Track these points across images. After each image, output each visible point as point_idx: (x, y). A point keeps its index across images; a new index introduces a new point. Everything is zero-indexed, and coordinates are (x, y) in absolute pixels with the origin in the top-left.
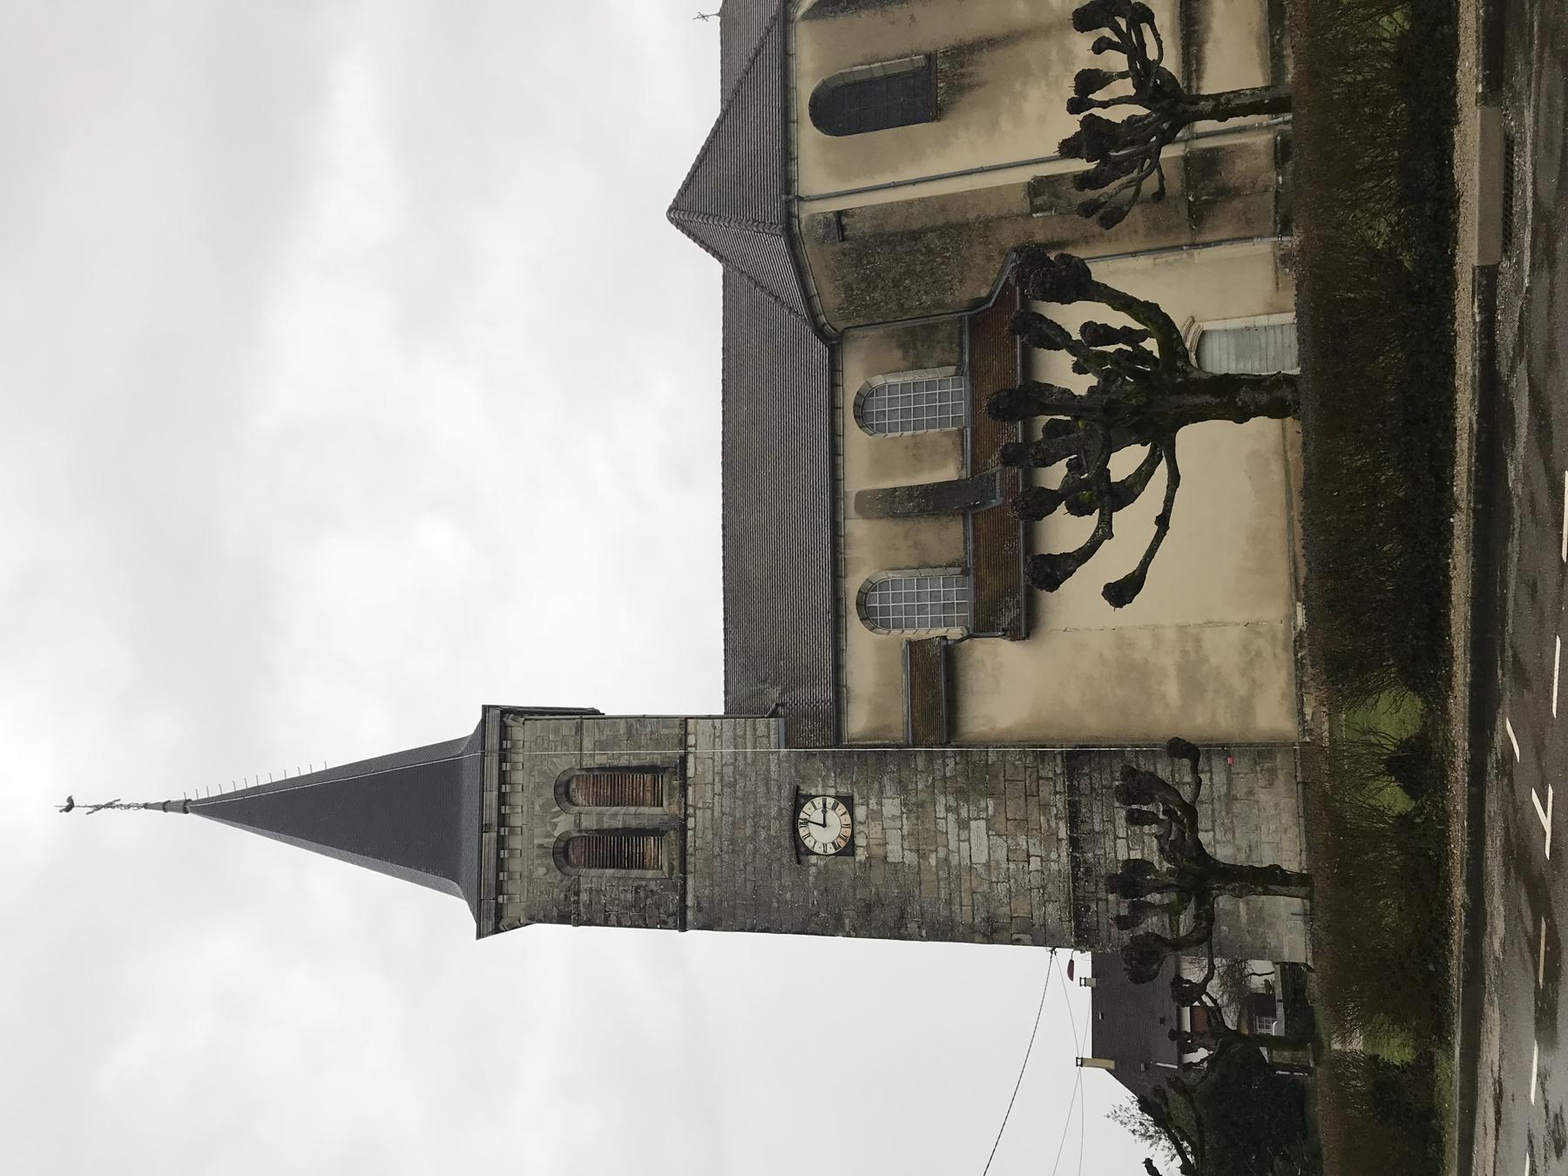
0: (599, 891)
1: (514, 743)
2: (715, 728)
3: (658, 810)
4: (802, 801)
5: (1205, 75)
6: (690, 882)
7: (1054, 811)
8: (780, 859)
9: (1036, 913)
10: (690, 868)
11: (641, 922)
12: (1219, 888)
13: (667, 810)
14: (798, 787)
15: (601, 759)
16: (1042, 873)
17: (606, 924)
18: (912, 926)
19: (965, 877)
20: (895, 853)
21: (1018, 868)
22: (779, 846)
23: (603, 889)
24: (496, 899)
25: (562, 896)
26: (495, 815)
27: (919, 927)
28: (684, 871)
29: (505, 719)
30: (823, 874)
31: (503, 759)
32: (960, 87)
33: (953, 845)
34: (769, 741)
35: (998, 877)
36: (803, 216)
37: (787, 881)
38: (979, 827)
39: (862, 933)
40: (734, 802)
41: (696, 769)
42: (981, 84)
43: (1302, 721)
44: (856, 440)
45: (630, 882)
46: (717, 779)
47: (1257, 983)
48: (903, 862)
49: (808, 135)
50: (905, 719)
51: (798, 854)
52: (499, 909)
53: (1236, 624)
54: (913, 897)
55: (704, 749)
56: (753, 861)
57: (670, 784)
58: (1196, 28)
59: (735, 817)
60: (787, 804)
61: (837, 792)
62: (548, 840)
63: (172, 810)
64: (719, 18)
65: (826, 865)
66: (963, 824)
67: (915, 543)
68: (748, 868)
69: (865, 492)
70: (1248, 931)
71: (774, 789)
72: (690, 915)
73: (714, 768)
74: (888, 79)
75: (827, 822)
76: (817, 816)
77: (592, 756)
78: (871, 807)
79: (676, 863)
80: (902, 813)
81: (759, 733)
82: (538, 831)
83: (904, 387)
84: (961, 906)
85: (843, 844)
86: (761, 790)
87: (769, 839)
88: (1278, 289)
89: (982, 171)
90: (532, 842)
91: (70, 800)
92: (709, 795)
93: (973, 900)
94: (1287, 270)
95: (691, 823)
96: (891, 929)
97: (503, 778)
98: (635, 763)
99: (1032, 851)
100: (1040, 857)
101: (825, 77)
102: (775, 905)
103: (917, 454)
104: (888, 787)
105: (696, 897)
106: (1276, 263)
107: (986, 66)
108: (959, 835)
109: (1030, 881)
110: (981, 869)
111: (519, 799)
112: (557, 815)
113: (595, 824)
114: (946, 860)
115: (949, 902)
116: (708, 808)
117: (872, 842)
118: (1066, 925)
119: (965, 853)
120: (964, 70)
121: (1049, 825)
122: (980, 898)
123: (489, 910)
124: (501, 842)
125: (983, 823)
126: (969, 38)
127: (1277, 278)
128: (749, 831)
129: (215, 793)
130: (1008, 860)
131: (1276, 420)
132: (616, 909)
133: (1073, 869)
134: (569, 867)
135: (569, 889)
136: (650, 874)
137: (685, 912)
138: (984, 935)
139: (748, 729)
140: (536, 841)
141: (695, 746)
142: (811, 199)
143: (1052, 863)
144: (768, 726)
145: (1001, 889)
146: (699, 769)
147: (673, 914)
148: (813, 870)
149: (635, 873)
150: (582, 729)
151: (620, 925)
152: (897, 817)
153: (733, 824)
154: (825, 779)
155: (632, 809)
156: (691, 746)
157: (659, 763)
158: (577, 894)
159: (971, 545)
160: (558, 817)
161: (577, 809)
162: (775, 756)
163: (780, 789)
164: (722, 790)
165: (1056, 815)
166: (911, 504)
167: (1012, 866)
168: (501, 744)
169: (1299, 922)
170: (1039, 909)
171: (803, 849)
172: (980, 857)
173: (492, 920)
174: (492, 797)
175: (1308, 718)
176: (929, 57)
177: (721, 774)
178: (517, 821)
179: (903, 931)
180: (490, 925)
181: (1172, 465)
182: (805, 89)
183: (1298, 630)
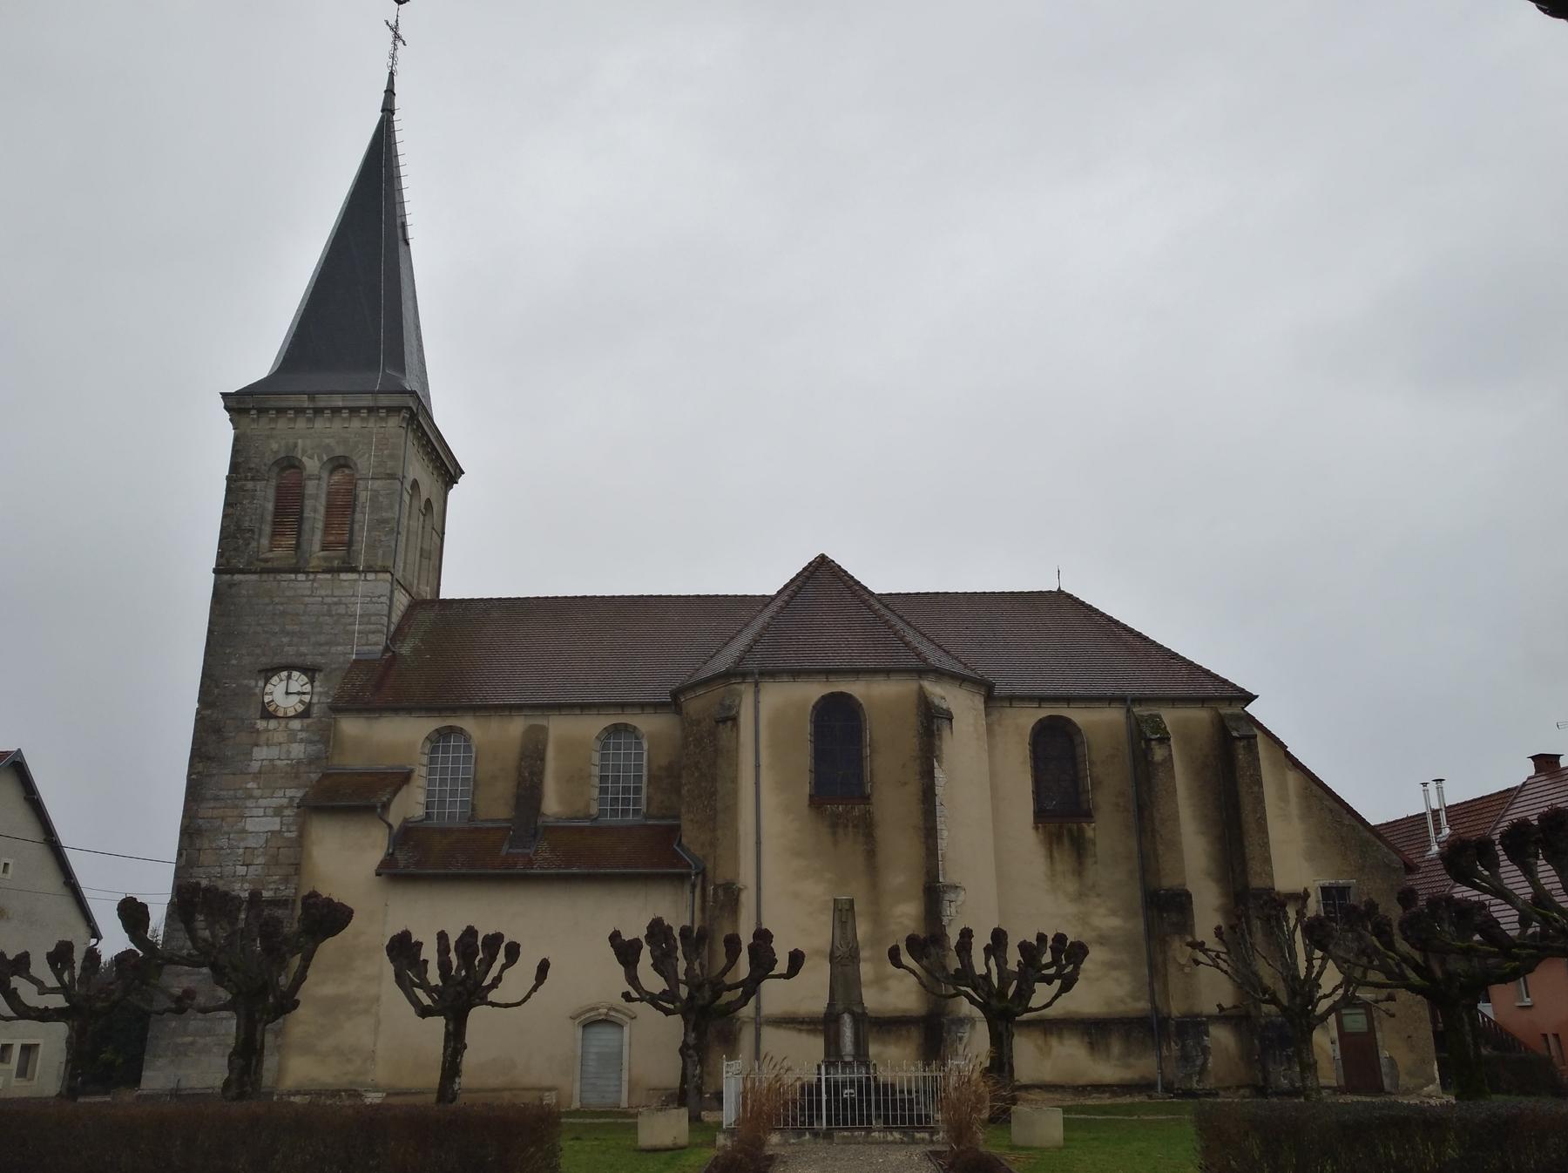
0: (253, 498)
2: (379, 597)
3: (316, 547)
4: (310, 674)
6: (254, 577)
7: (282, 888)
9: (201, 870)
10: (265, 577)
12: (73, 1026)
13: (315, 556)
14: (320, 671)
15: (363, 496)
16: (233, 877)
18: (200, 767)
19: (236, 812)
20: (261, 753)
23: (255, 502)
24: (253, 408)
25: (253, 466)
26: (322, 404)
27: (199, 773)
28: (263, 571)
29: (404, 411)
31: (371, 410)
32: (835, 824)
33: (263, 802)
34: (363, 645)
36: (743, 687)
38: (274, 822)
41: (345, 581)
43: (290, 1094)
44: (592, 726)
45: (258, 525)
47: (1439, 1029)
48: (251, 760)
49: (814, 691)
51: (267, 670)
52: (246, 411)
55: (361, 588)
56: (266, 632)
57: (335, 558)
59: (302, 616)
60: (309, 660)
61: (314, 704)
62: (300, 451)
64: (1056, 590)
65: (255, 694)
66: (278, 812)
69: (547, 734)
70: (169, 1044)
71: (322, 650)
72: (227, 577)
73: (346, 596)
75: (290, 696)
77: (366, 489)
78: (299, 733)
79: (269, 565)
80: (292, 760)
81: (370, 636)
83: (638, 767)
84: (213, 808)
85: (271, 709)
86: (322, 639)
88: (650, 1090)
89: (758, 843)
90: (300, 438)
92: (323, 593)
93: (215, 818)
94: (664, 1098)
95: (301, 577)
97: (354, 411)
98: (356, 527)
99: (251, 868)
100: (246, 875)
101: (864, 706)
104: (314, 748)
105: (240, 582)
106: (671, 1089)
108: (270, 807)
110: (240, 825)
111: (337, 425)
112: (320, 459)
113: (310, 492)
114: (251, 797)
115: (216, 798)
116: (312, 592)
119: (255, 812)
120: (850, 829)
121: (271, 883)
124: (300, 411)
125: (277, 827)
127: (659, 1089)
128: (289, 628)
129: (398, 136)
130: (246, 848)
131: (438, 1080)
132: (238, 513)
135: (258, 471)
136: (265, 542)
138: (187, 826)
139: (375, 626)
140: (300, 441)
141: (366, 580)
142: (757, 693)
144: (376, 644)
145: (224, 842)
146: (346, 584)
147: (228, 562)
148: (253, 683)
149: (267, 529)
150: (392, 479)
151: (225, 516)
152: (288, 756)
153: (298, 614)
154: (326, 693)
155: (320, 525)
156: (365, 576)
157: (353, 548)
158: (253, 479)
159: (489, 825)
160: (319, 460)
161: (325, 475)
162: (349, 651)
163: (322, 655)
164: (325, 604)
165: (279, 889)
166: (527, 774)
169: (172, 1085)
170: (204, 873)
171: (269, 674)
172: (250, 825)
173: (239, 404)
174: (338, 401)
176: (866, 799)
178: (319, 424)
180: (235, 405)
181: (33, 1014)
182: (856, 688)
183: (364, 1094)
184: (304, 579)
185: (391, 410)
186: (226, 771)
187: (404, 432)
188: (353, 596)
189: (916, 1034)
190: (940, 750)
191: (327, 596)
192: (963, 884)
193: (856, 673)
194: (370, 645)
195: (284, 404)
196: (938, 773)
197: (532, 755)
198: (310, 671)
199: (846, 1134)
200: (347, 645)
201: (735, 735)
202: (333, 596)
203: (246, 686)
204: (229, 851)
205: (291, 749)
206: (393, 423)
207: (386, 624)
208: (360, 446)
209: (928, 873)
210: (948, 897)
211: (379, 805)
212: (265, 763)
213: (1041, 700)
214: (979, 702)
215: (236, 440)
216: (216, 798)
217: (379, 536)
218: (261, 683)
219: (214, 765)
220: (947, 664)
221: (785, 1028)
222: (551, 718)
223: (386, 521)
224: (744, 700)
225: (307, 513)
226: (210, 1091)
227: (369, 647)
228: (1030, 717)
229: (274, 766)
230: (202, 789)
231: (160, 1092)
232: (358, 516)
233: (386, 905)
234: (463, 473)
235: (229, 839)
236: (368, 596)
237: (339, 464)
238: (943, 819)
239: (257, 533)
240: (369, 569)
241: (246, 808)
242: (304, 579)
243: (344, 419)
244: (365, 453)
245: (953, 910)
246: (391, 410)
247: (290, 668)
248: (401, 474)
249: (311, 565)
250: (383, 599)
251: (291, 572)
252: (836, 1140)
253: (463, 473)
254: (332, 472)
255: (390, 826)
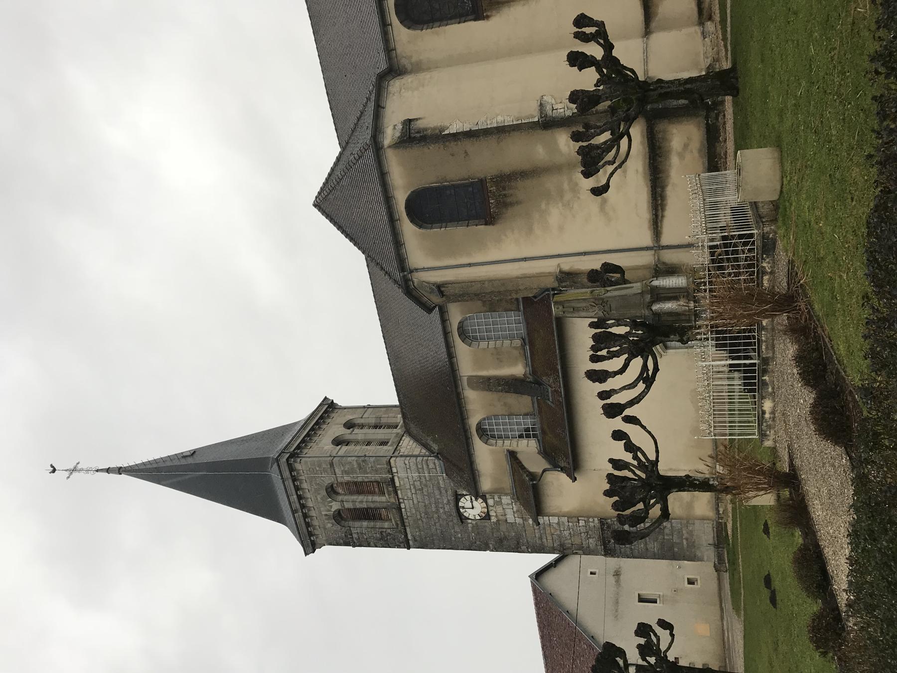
1: (298, 471)
2: (406, 464)
3: (383, 499)
5: (667, 208)
6: (408, 530)
8: (452, 521)
10: (407, 524)
11: (387, 545)
14: (456, 491)
15: (347, 478)
16: (586, 527)
17: (369, 546)
18: (524, 548)
19: (548, 528)
20: (510, 518)
21: (574, 526)
22: (451, 515)
24: (310, 539)
25: (343, 535)
30: (476, 527)
32: (505, 204)
35: (564, 528)
36: (415, 280)
37: (457, 529)
39: (499, 550)
40: (424, 498)
41: (400, 483)
42: (518, 203)
46: (412, 487)
48: (516, 523)
49: (408, 228)
50: (511, 485)
51: (461, 519)
53: (685, 470)
54: (523, 536)
55: (402, 474)
58: (660, 175)
60: (451, 498)
63: (112, 473)
67: (504, 403)
68: (437, 524)
71: (443, 492)
72: (411, 543)
74: (454, 187)
75: (474, 506)
76: (468, 504)
78: (495, 499)
80: (512, 502)
81: (430, 467)
82: (322, 509)
84: (547, 540)
85: (484, 515)
86: (437, 492)
87: (445, 513)
89: (525, 259)
91: (52, 466)
92: (409, 494)
95: (403, 506)
96: (513, 549)
97: (297, 489)
102: (453, 539)
103: (499, 357)
107: (521, 190)
109: (580, 530)
112: (330, 502)
115: (541, 538)
116: (410, 499)
117: (498, 514)
118: (599, 547)
122: (556, 537)
123: (308, 544)
124: (305, 516)
126: (507, 170)
128: (434, 510)
133: (601, 526)
134: (343, 522)
136: (386, 525)
137: (409, 543)
139: (424, 465)
140: (323, 513)
141: (397, 472)
142: (417, 270)
143: (591, 523)
145: (566, 533)
146: (402, 482)
147: (403, 542)
148: (470, 525)
149: (379, 524)
150: (333, 465)
152: (510, 504)
153: (425, 506)
155: (370, 498)
159: (538, 444)
161: (340, 498)
163: (446, 491)
167: (570, 524)
168: (291, 474)
169: (712, 548)
170: (586, 541)
171: (463, 518)
173: (310, 545)
174: (294, 497)
175: (721, 512)
176: (482, 182)
177: (414, 485)
178: (310, 504)
179: (519, 549)
182: (401, 198)
184: (403, 504)
185: (291, 469)
186: (524, 534)
187: (303, 459)
188: (408, 478)
189: (661, 126)
190: (434, 129)
191: (411, 492)
192: (538, 98)
193: (388, 199)
194: (436, 466)
195: (304, 525)
196: (453, 130)
197: (487, 384)
198: (457, 498)
199: (764, 347)
200: (438, 479)
201: (450, 285)
202: (410, 489)
203: (472, 528)
204: (571, 530)
205: (506, 503)
206: (298, 466)
207: (421, 458)
208: (318, 482)
209: (532, 128)
210: (549, 113)
211: (531, 483)
212: (516, 515)
213: (385, 24)
214: (395, 85)
215: (330, 544)
216: (541, 538)
217: (369, 468)
218: (470, 521)
219: (521, 541)
220: (368, 119)
221: (661, 227)
222: (462, 375)
223: (359, 464)
224: (424, 280)
225: (365, 505)
226: (715, 529)
227: (437, 467)
228: (401, 33)
229: (518, 511)
230: (537, 546)
231: (716, 553)
232: (360, 479)
233: (595, 470)
234: (326, 398)
235: (564, 531)
236: (407, 471)
237: (331, 491)
238: (488, 122)
239: (382, 530)
240: (390, 471)
241: (544, 523)
242: (403, 504)
243: (304, 493)
244: (321, 480)
245: (559, 106)
246: (291, 469)
247: (457, 508)
248: (330, 458)
249: (394, 501)
250: (407, 462)
251: (401, 511)
252: (770, 355)
253: (326, 398)
254: (337, 493)
255: (544, 471)
